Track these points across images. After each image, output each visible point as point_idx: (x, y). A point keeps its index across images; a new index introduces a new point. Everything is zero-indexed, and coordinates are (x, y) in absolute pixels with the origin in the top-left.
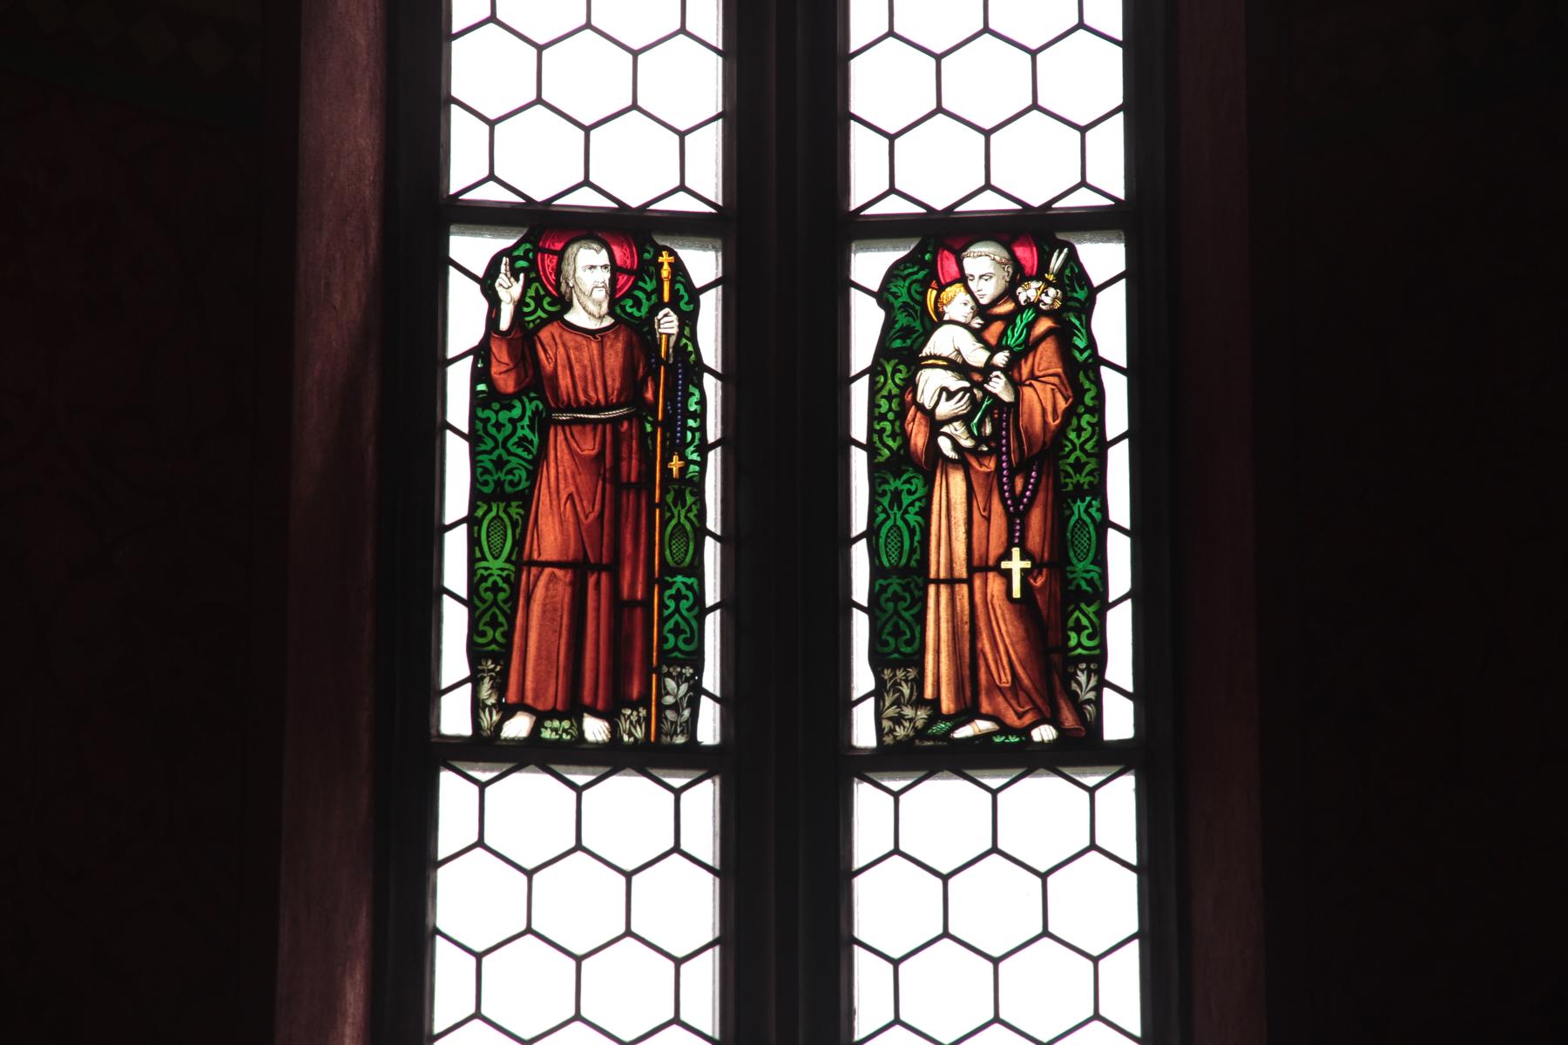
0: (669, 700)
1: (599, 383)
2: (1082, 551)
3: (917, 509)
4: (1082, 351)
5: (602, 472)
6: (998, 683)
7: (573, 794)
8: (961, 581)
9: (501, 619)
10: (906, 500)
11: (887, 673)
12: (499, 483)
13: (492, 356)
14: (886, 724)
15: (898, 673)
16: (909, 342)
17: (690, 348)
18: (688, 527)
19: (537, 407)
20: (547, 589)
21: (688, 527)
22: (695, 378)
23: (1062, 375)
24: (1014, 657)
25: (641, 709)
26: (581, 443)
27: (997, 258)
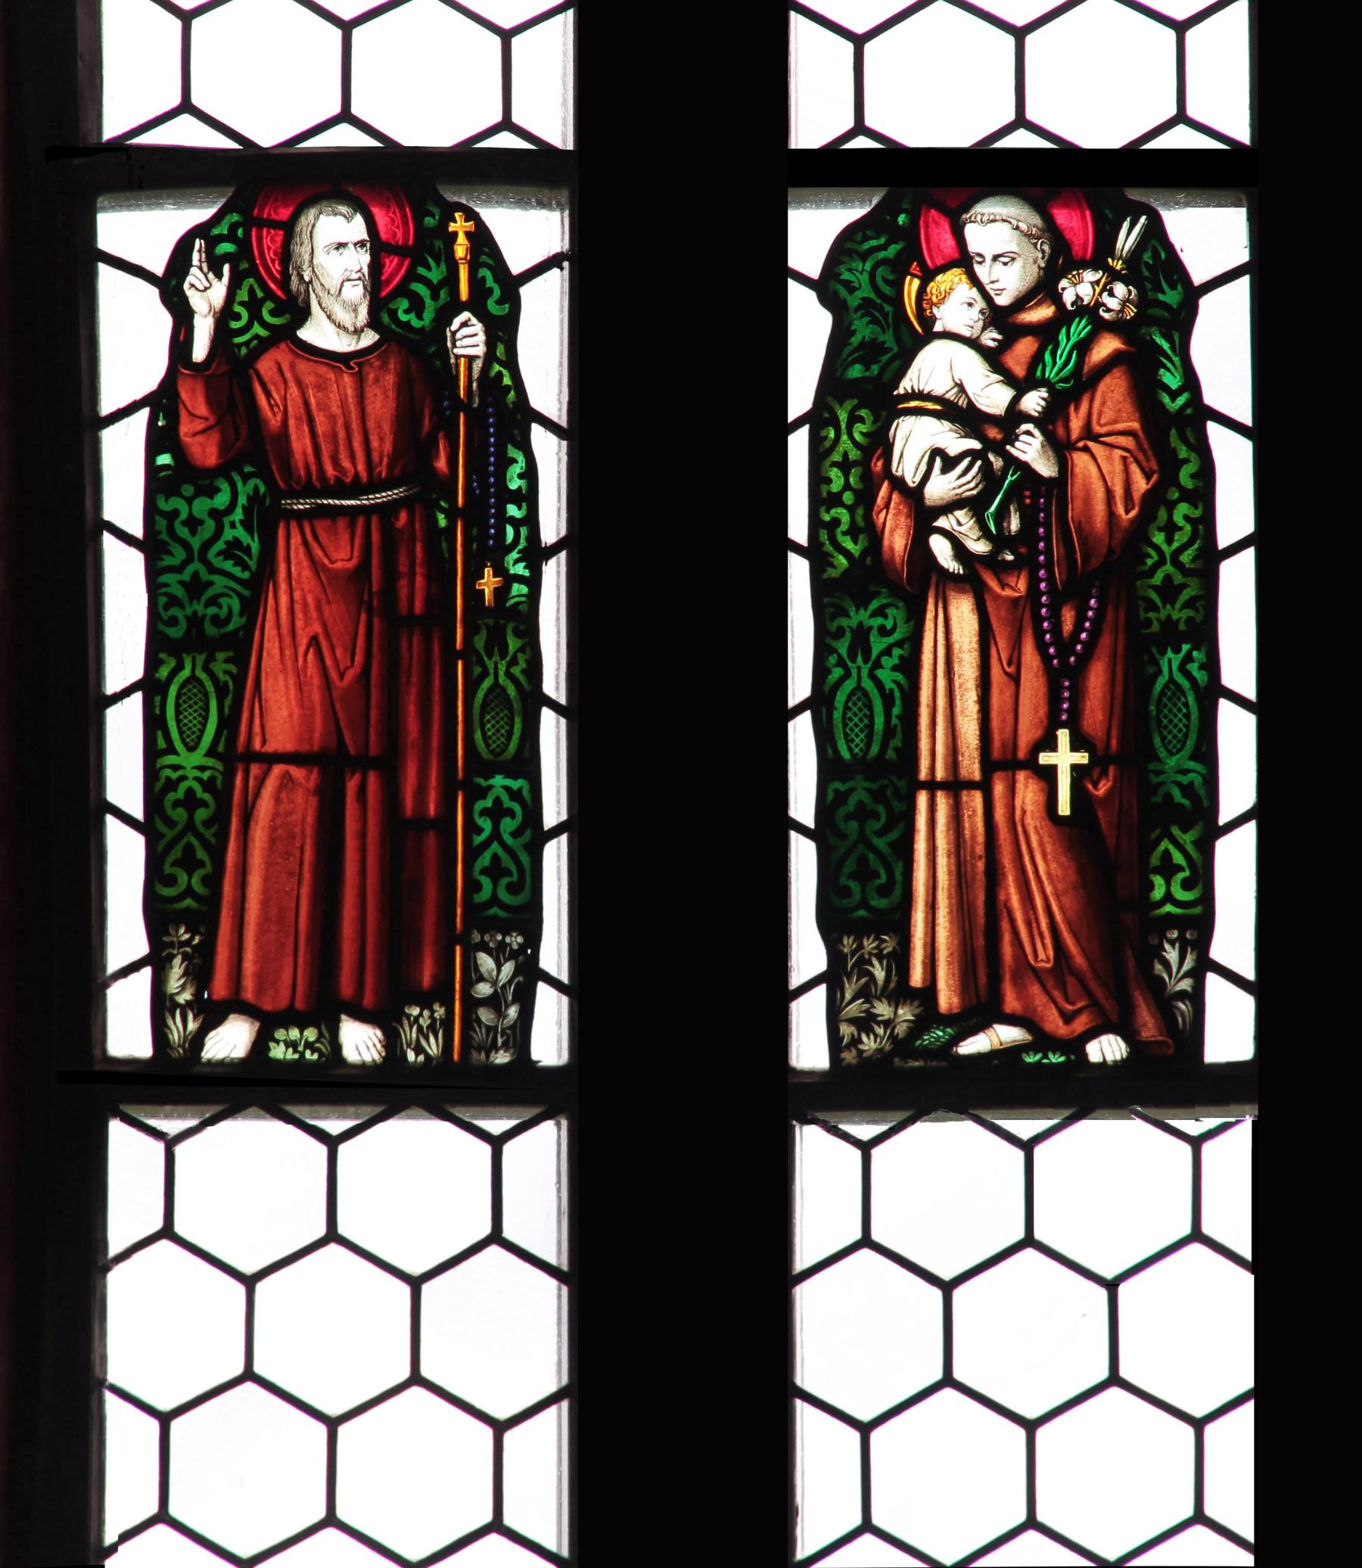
0: (484, 989)
1: (357, 444)
2: (1175, 737)
3: (896, 661)
4: (1174, 395)
5: (366, 598)
6: (1032, 962)
7: (322, 1150)
8: (971, 785)
9: (201, 854)
10: (878, 644)
11: (848, 943)
12: (195, 621)
13: (181, 406)
14: (846, 1030)
15: (865, 943)
16: (875, 368)
17: (507, 381)
18: (511, 691)
19: (256, 488)
20: (277, 800)
21: (511, 691)
22: (516, 432)
23: (1140, 433)
24: (1058, 917)
25: (436, 1007)
26: (330, 549)
27: (1023, 226)
